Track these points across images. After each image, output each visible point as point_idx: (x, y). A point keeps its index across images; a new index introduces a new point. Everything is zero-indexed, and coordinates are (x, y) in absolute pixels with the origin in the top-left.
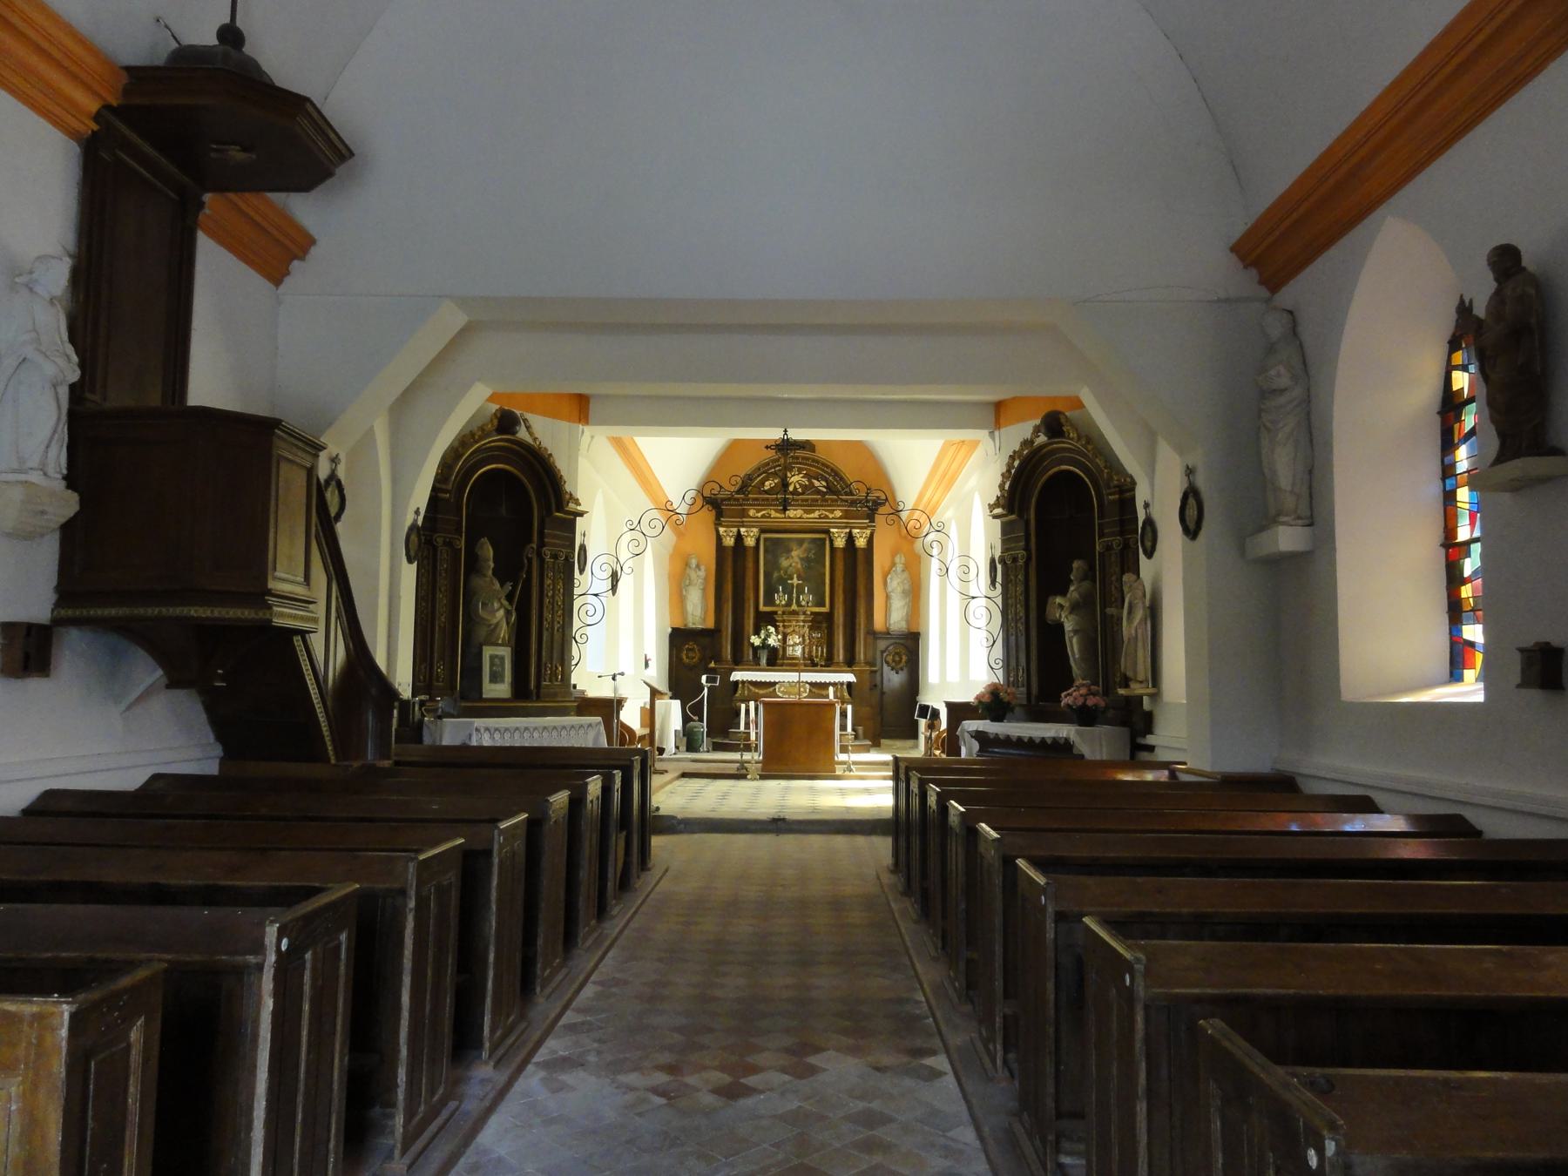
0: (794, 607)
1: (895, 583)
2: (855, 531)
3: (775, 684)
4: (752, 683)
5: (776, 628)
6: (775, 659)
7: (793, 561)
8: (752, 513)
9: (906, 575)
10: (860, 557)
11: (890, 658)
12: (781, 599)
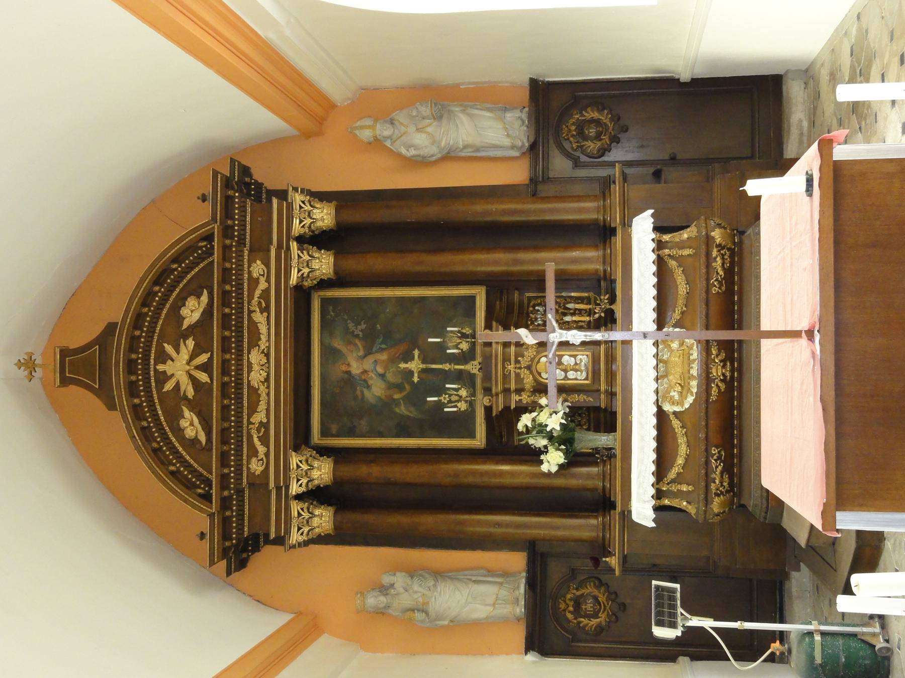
0: (473, 367)
1: (420, 139)
2: (297, 229)
3: (661, 414)
4: (660, 472)
5: (523, 409)
6: (597, 413)
7: (372, 371)
8: (256, 467)
9: (401, 117)
10: (356, 216)
11: (592, 146)
12: (456, 399)
